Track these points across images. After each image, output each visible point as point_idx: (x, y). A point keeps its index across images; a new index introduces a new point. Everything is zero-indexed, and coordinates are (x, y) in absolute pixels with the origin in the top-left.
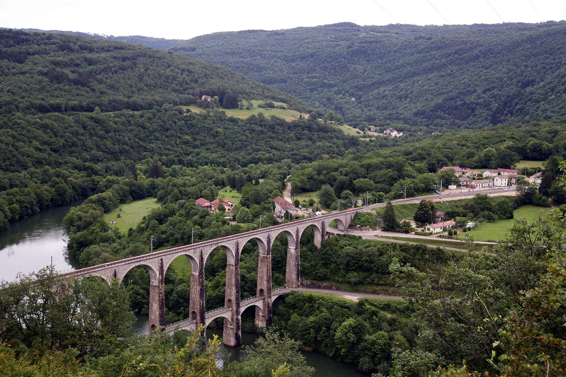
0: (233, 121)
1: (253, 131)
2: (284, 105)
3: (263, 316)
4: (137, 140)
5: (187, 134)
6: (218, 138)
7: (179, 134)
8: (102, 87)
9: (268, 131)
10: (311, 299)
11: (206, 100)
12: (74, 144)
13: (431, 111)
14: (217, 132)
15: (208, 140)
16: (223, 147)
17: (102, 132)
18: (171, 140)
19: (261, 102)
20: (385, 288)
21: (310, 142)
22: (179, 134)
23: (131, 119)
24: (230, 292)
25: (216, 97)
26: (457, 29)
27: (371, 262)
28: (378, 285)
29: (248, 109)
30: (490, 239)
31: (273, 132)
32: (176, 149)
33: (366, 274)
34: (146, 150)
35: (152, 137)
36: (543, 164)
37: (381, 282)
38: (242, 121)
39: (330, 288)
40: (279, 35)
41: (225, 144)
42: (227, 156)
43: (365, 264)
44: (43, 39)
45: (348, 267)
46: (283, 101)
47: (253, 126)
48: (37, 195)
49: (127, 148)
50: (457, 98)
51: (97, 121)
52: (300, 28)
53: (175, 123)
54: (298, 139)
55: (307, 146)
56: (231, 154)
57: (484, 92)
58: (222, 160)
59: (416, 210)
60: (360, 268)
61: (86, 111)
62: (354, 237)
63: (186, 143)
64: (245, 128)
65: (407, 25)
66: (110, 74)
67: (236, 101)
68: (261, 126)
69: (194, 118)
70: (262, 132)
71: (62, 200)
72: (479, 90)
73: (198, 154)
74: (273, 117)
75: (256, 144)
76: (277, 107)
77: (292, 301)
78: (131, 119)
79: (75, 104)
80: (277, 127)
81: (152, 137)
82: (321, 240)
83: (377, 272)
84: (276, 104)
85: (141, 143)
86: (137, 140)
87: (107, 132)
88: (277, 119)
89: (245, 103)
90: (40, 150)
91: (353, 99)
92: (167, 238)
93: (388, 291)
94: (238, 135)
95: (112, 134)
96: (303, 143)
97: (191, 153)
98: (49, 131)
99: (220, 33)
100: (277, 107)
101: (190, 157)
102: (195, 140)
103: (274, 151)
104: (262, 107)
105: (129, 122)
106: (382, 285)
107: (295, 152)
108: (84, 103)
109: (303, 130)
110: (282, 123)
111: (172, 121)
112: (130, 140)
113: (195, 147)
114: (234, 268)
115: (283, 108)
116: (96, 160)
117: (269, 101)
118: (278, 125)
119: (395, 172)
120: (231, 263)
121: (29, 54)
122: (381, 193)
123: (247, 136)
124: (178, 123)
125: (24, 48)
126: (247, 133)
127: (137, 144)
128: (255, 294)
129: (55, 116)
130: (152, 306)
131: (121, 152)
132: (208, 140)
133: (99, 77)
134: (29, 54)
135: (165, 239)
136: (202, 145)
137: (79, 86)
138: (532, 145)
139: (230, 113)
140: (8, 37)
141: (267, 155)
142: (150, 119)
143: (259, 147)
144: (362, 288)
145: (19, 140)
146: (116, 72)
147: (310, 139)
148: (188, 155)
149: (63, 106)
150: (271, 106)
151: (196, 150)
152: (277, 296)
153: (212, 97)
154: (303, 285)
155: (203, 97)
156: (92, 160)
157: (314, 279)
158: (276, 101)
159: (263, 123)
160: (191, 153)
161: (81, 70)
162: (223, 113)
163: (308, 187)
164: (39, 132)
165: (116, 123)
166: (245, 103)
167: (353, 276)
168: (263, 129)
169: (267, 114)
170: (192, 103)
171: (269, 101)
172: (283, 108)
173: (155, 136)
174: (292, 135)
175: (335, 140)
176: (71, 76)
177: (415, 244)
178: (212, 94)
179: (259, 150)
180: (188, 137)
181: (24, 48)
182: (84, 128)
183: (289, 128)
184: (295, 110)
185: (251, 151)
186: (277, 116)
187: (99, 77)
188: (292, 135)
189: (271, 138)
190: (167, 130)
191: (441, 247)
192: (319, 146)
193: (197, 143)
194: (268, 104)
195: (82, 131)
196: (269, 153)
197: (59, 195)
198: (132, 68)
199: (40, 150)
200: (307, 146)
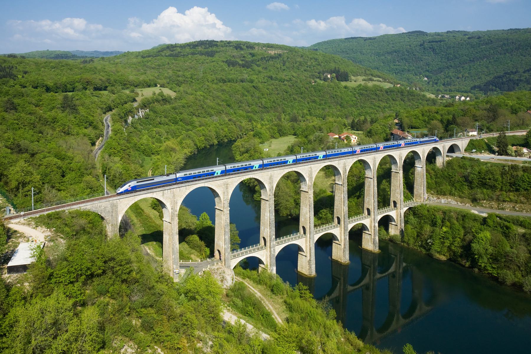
2: (381, 79)
8: (260, 69)
13: (484, 86)
19: (364, 77)
26: (496, 32)
40: (372, 39)
42: (343, 111)
44: (225, 44)
46: (379, 77)
48: (216, 132)
50: (504, 76)
52: (386, 35)
57: (524, 72)
65: (330, 41)
66: (265, 61)
67: (348, 77)
72: (521, 70)
76: (376, 81)
84: (375, 79)
89: (353, 78)
90: (220, 105)
99: (333, 40)
110: (381, 89)
113: (320, 105)
115: (380, 81)
117: (370, 77)
121: (217, 52)
125: (214, 49)
128: (389, 205)
133: (258, 63)
134: (217, 52)
139: (344, 84)
140: (206, 43)
145: (207, 99)
146: (268, 60)
150: (371, 80)
152: (408, 208)
153: (331, 74)
158: (375, 77)
161: (247, 60)
164: (219, 94)
169: (370, 84)
172: (380, 81)
175: (421, 101)
176: (241, 62)
178: (331, 72)
181: (214, 49)
183: (387, 92)
184: (388, 82)
187: (258, 63)
190: (302, 93)
198: (278, 58)
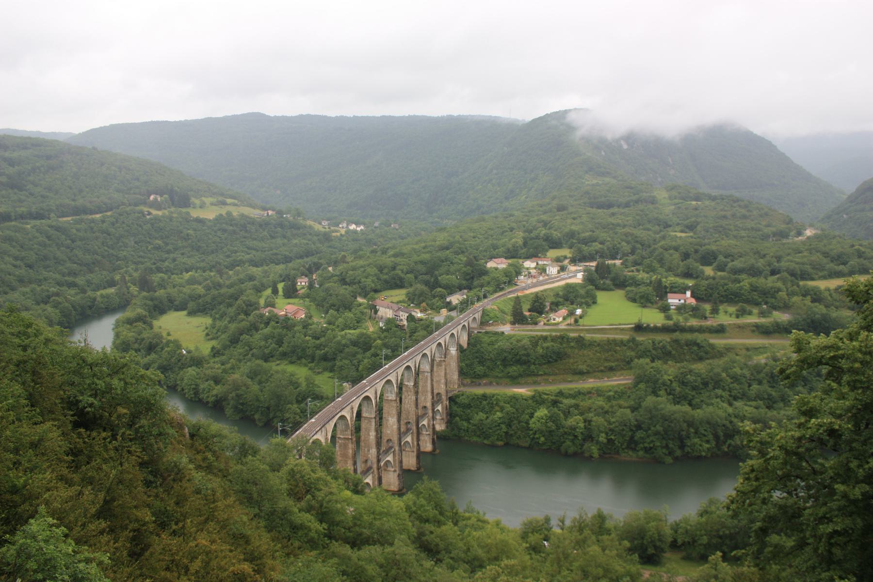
0: (199, 221)
1: (225, 231)
2: (236, 201)
3: (442, 419)
4: (106, 248)
5: (156, 238)
6: (190, 241)
7: (148, 240)
9: (241, 231)
10: (485, 397)
11: (156, 199)
12: (45, 258)
14: (188, 235)
15: (180, 243)
16: (198, 250)
17: (69, 242)
18: (141, 247)
20: (546, 377)
21: (286, 241)
22: (148, 240)
23: (92, 225)
24: (425, 399)
25: (165, 196)
27: (528, 355)
28: (538, 375)
29: (201, 207)
30: (612, 322)
31: (246, 231)
32: (149, 255)
33: (525, 367)
34: (118, 259)
35: (121, 244)
36: (570, 253)
37: (540, 373)
38: (210, 220)
39: (491, 384)
41: (199, 246)
43: (524, 358)
45: (505, 363)
47: (224, 225)
49: (99, 258)
51: (58, 229)
53: (141, 226)
54: (272, 237)
55: (284, 245)
56: (210, 258)
58: (202, 265)
59: (512, 303)
60: (519, 362)
61: (35, 218)
62: (496, 333)
63: (158, 248)
64: (215, 228)
68: (231, 225)
69: (160, 221)
70: (234, 232)
71: (68, 322)
73: (174, 260)
74: (242, 215)
75: (231, 245)
76: (230, 204)
77: (466, 401)
78: (92, 225)
79: (23, 212)
80: (248, 226)
81: (121, 244)
82: (467, 339)
83: (534, 364)
84: (229, 201)
85: (111, 251)
86: (106, 248)
87: (73, 241)
88: (247, 217)
91: (278, 192)
92: (271, 353)
93: (548, 380)
94: (210, 236)
95: (79, 243)
96: (279, 241)
97: (166, 259)
98: (14, 244)
100: (230, 204)
101: (167, 264)
102: (167, 244)
103: (254, 252)
104: (215, 205)
105: (92, 228)
106: (541, 375)
107: (275, 251)
108: (33, 210)
109: (276, 228)
111: (137, 225)
112: (99, 248)
113: (168, 252)
114: (429, 374)
116: (74, 274)
118: (249, 223)
119: (468, 267)
120: (425, 370)
122: (33, 286)
123: (220, 237)
124: (145, 227)
126: (219, 233)
127: (107, 253)
129: (14, 226)
130: (388, 420)
131: (94, 263)
132: (180, 243)
135: (269, 354)
136: (176, 249)
137: (16, 190)
138: (544, 235)
141: (248, 256)
142: (113, 224)
143: (236, 248)
144: (522, 380)
147: (284, 237)
148: (164, 261)
149: (13, 214)
150: (224, 203)
151: (172, 255)
153: (161, 196)
154: (464, 385)
155: (152, 197)
156: (69, 274)
157: (475, 377)
159: (233, 222)
160: (166, 259)
162: (188, 213)
163: (379, 287)
165: (78, 230)
166: (197, 202)
167: (514, 369)
168: (235, 228)
170: (141, 204)
171: (220, 198)
173: (123, 242)
174: (265, 233)
175: (309, 237)
177: (558, 334)
179: (236, 252)
180: (160, 242)
182: (49, 238)
183: (261, 226)
185: (229, 253)
186: (246, 213)
188: (265, 233)
189: (245, 237)
191: (582, 335)
192: (296, 244)
193: (170, 247)
194: (220, 202)
195: (48, 242)
196: (249, 254)
197: (65, 316)
199: (15, 266)
200: (284, 245)
